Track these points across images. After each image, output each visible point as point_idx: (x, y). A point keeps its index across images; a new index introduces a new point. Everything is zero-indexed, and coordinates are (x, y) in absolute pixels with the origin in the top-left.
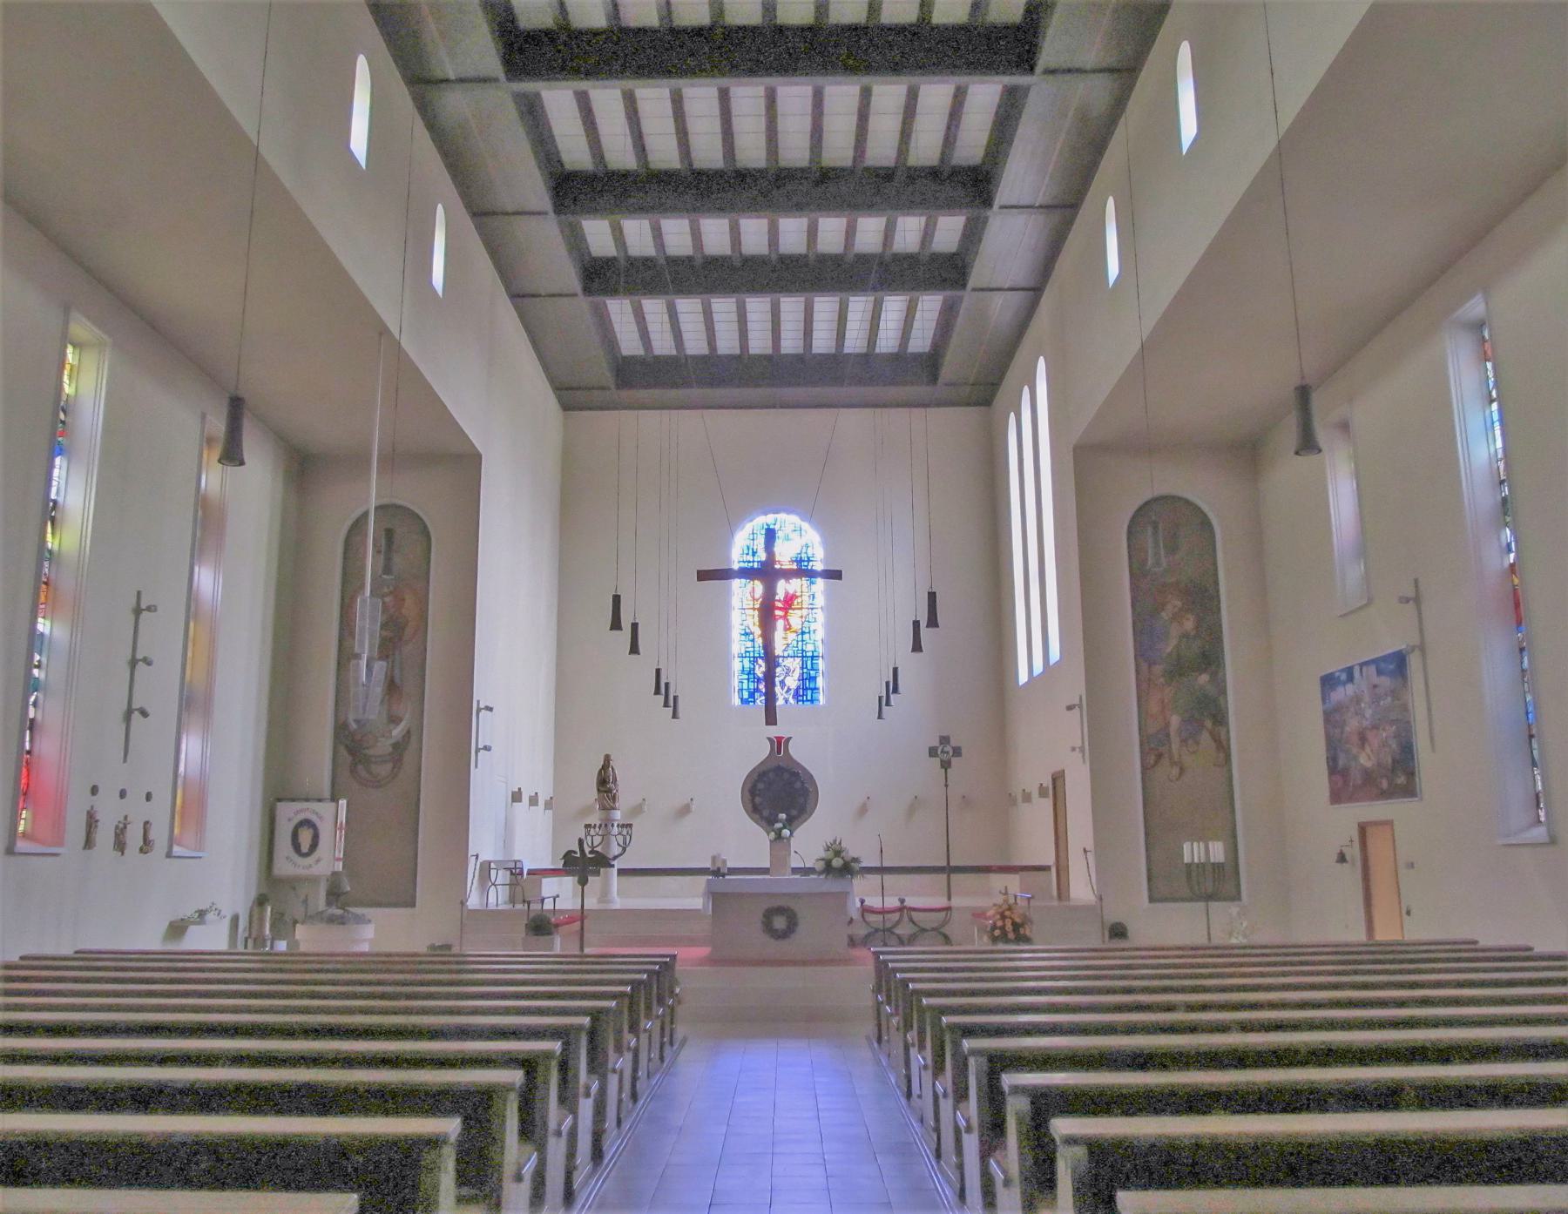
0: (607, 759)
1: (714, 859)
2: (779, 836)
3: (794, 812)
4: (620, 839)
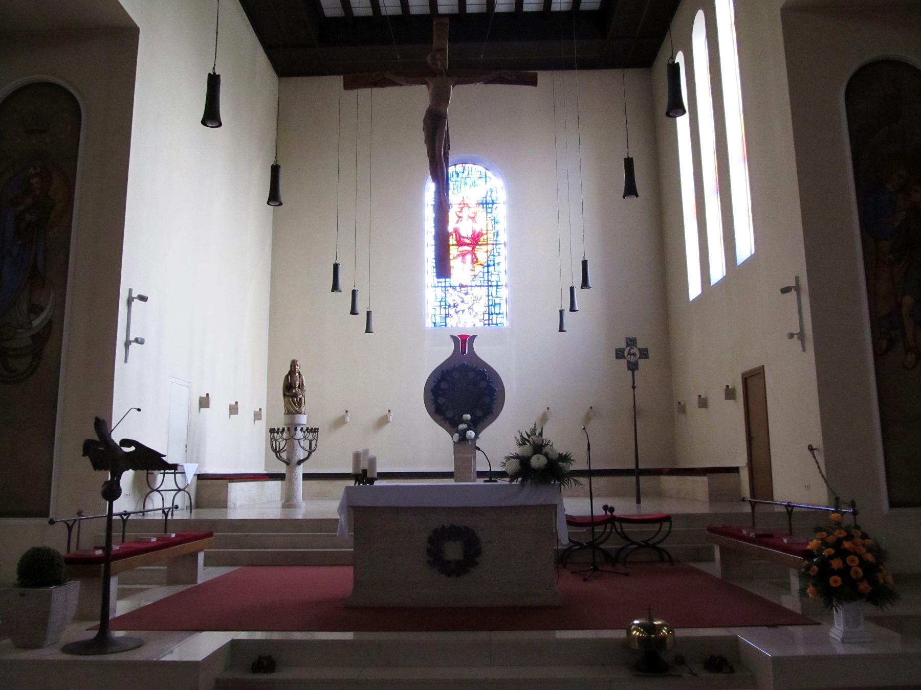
0: (294, 364)
1: (357, 457)
2: (463, 438)
3: (479, 413)
4: (306, 444)
